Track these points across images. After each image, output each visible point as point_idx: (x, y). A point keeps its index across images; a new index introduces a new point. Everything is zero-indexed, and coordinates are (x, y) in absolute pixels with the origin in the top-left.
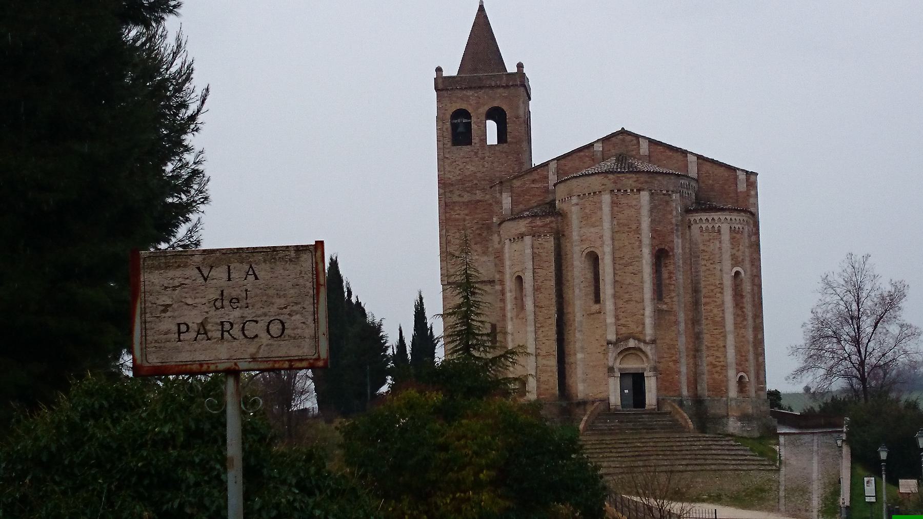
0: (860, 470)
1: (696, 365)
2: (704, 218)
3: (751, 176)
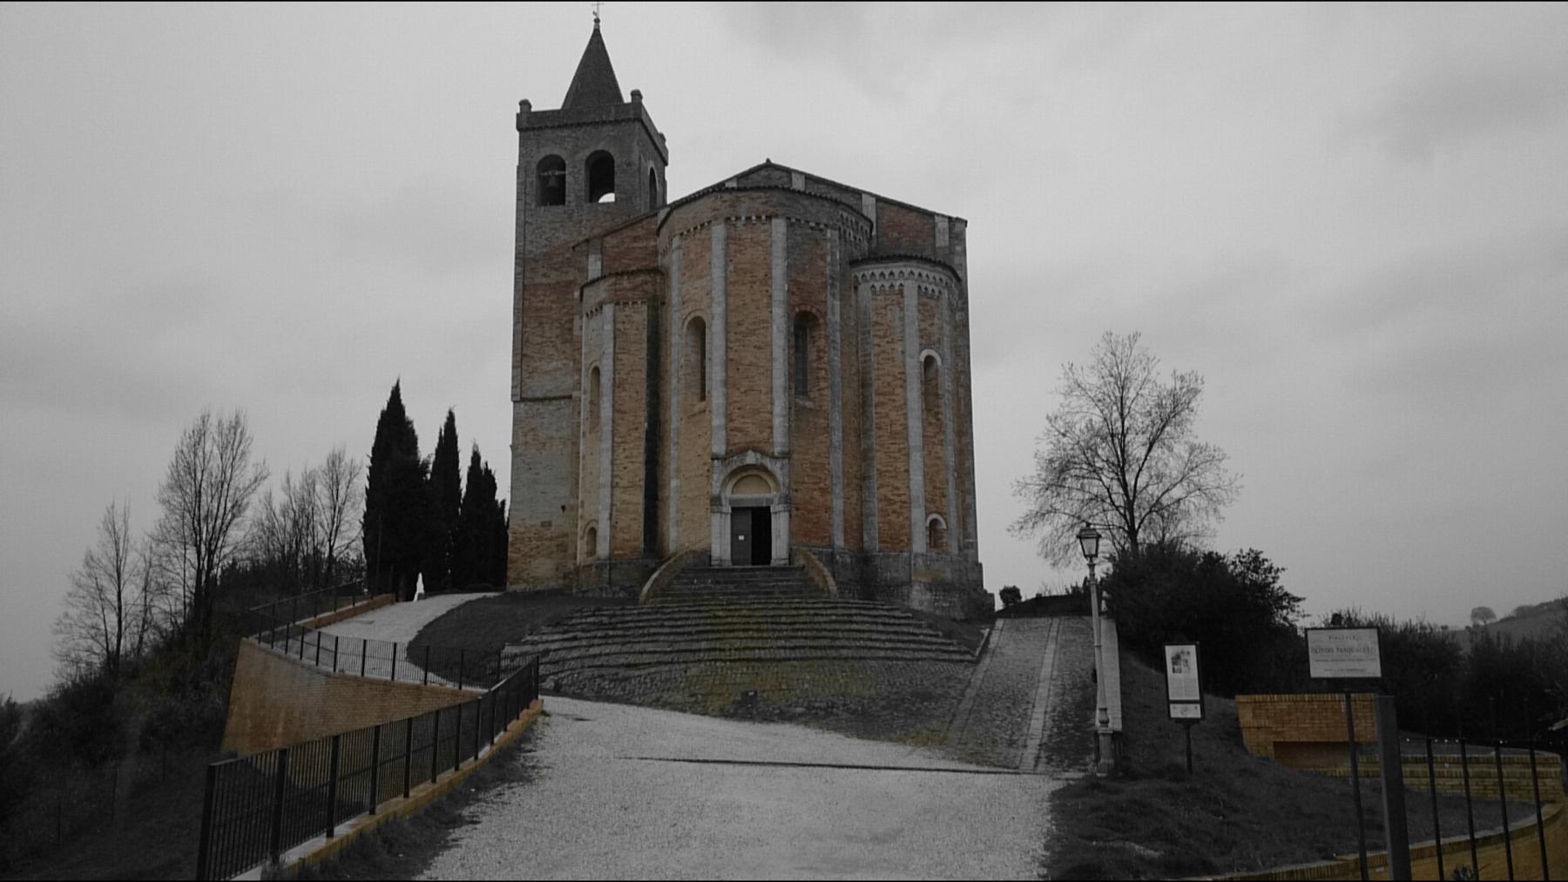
0: (1134, 662)
1: (862, 502)
2: (878, 272)
3: (956, 227)
